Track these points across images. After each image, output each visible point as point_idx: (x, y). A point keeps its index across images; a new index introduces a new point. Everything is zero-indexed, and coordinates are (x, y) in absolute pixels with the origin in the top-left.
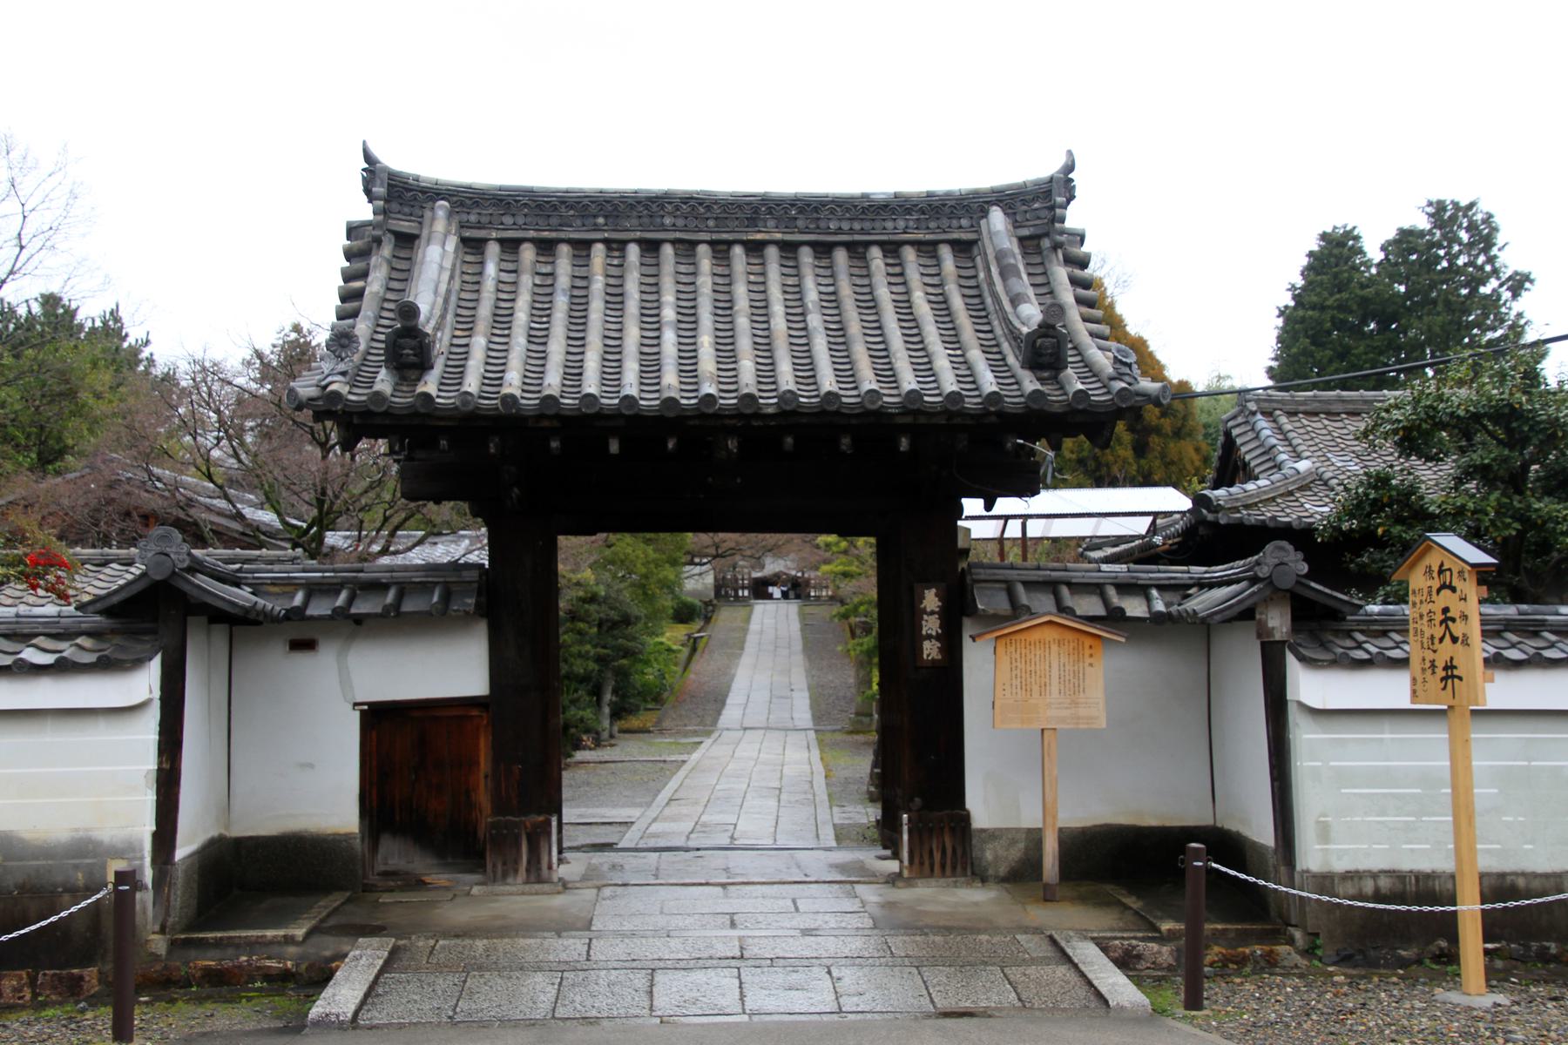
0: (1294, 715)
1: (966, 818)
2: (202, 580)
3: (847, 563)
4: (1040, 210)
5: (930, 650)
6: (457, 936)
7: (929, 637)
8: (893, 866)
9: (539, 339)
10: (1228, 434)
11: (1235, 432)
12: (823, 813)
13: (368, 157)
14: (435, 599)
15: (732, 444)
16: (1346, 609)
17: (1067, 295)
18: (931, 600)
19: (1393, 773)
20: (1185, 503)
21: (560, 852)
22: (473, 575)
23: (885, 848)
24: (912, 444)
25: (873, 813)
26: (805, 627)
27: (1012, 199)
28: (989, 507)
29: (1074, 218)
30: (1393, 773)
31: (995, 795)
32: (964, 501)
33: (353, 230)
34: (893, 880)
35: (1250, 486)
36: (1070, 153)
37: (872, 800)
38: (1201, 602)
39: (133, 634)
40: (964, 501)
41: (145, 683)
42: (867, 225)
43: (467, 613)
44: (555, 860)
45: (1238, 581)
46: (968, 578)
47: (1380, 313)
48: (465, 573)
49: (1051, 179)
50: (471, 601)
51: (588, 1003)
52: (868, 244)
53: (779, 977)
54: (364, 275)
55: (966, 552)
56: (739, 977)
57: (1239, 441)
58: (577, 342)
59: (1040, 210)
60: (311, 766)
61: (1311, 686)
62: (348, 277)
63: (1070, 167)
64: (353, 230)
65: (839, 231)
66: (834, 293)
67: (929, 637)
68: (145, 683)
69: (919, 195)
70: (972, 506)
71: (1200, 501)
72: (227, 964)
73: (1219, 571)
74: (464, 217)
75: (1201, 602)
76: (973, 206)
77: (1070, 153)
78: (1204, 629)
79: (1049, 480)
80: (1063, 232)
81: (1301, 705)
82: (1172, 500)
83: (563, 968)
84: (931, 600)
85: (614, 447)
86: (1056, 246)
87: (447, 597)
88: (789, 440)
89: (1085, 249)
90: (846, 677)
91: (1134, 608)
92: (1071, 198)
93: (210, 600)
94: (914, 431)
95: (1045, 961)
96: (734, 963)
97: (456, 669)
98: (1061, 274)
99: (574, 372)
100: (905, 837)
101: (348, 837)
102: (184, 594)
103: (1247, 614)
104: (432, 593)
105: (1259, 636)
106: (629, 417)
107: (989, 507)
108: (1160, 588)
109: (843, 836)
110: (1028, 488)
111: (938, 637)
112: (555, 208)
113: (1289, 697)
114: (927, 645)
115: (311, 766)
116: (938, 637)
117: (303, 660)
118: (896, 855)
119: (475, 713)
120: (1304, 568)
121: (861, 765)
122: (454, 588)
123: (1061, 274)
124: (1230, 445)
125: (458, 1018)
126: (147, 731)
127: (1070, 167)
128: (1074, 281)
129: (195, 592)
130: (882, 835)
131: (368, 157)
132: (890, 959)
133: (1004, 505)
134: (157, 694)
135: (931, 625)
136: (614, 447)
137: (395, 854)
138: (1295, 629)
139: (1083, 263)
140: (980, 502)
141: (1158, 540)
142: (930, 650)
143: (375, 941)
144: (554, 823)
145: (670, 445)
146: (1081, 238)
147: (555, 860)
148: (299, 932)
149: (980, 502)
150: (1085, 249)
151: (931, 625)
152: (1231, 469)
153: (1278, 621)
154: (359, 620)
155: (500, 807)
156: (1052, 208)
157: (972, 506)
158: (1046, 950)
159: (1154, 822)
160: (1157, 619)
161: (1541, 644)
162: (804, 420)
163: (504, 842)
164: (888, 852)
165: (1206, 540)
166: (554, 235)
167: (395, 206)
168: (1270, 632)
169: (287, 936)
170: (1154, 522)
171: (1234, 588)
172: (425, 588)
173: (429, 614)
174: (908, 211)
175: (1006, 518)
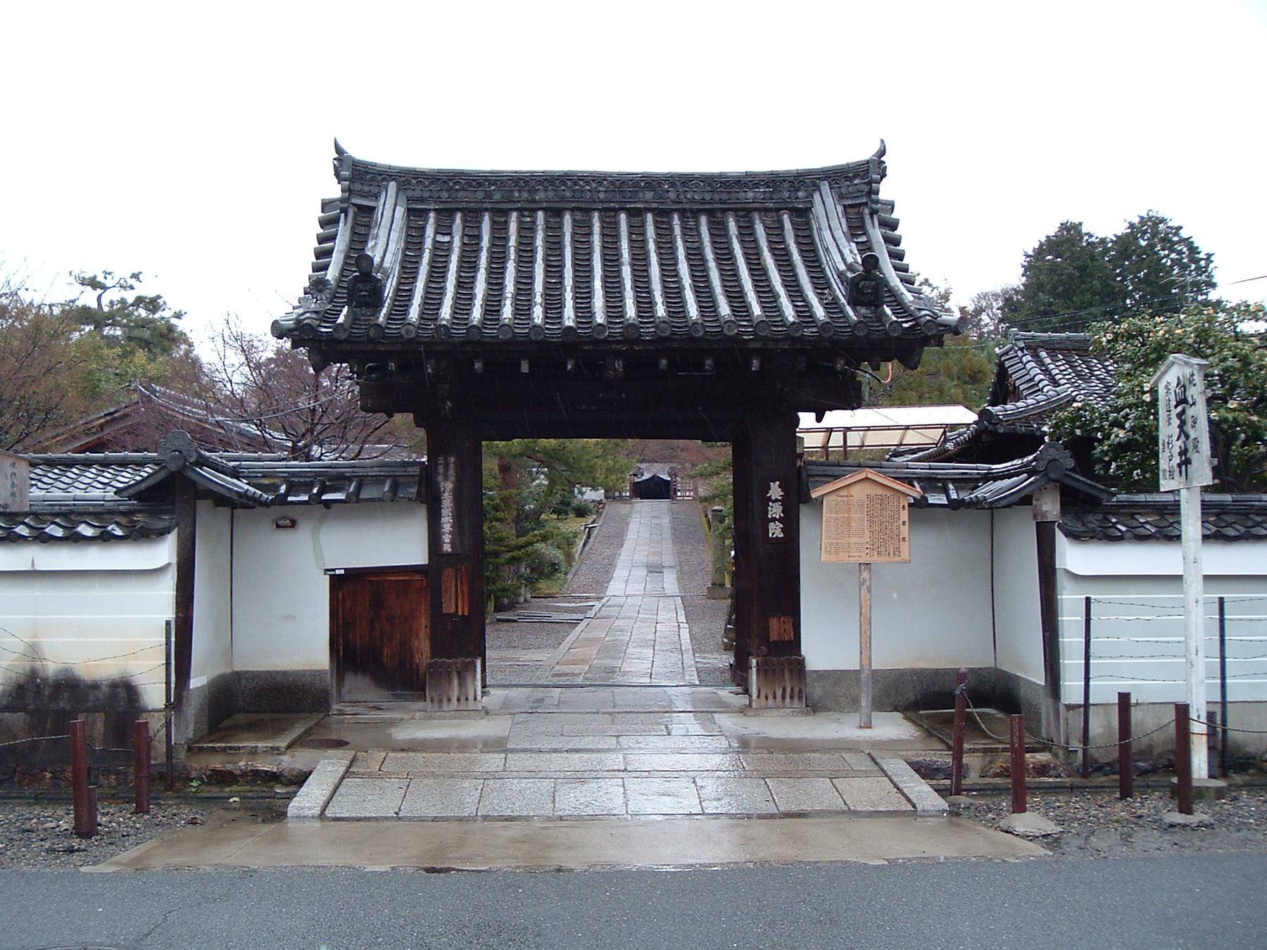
0: (1062, 582)
1: (801, 663)
2: (206, 472)
3: (703, 469)
4: (859, 186)
5: (775, 530)
6: (403, 750)
7: (774, 520)
8: (744, 700)
9: (465, 285)
10: (1001, 365)
11: (1007, 364)
12: (689, 659)
13: (338, 149)
14: (386, 489)
15: (619, 365)
16: (1102, 496)
17: (882, 252)
18: (775, 491)
19: (1157, 623)
20: (969, 417)
21: (484, 687)
22: (416, 471)
23: (738, 685)
24: (761, 365)
25: (728, 659)
26: (674, 520)
27: (837, 176)
28: (819, 419)
29: (886, 191)
30: (1157, 623)
31: (825, 643)
32: (800, 414)
33: (326, 205)
34: (742, 711)
35: (1020, 404)
36: (882, 141)
37: (727, 648)
38: (986, 491)
39: (155, 514)
40: (800, 414)
41: (164, 552)
42: (725, 196)
43: (410, 499)
44: (479, 693)
45: (1017, 475)
46: (804, 475)
47: (1108, 285)
48: (409, 469)
49: (868, 162)
50: (414, 490)
51: (504, 805)
52: (724, 211)
53: (656, 784)
54: (332, 238)
55: (801, 455)
56: (623, 786)
57: (1010, 371)
58: (495, 283)
59: (859, 186)
60: (293, 618)
61: (1075, 557)
62: (321, 240)
63: (882, 152)
64: (326, 205)
65: (703, 201)
66: (698, 248)
67: (774, 520)
68: (164, 552)
69: (765, 174)
70: (807, 419)
71: (983, 414)
72: (229, 767)
73: (998, 467)
74: (410, 193)
75: (986, 491)
76: (805, 181)
77: (882, 141)
78: (991, 508)
79: (866, 397)
80: (877, 202)
81: (1067, 571)
82: (963, 415)
83: (488, 776)
84: (775, 491)
85: (525, 368)
86: (873, 213)
87: (395, 487)
88: (664, 362)
89: (894, 216)
90: (707, 556)
91: (936, 499)
92: (883, 176)
93: (212, 487)
94: (763, 354)
95: (866, 774)
96: (621, 774)
97: (399, 544)
98: (876, 234)
99: (492, 308)
100: (754, 677)
101: (321, 672)
102: (194, 483)
103: (1026, 500)
104: (384, 484)
105: (1035, 517)
106: (537, 342)
107: (819, 419)
108: (954, 481)
109: (705, 675)
110: (852, 402)
111: (780, 520)
112: (480, 184)
113: (1059, 565)
114: (771, 526)
115: (293, 618)
116: (780, 520)
117: (285, 537)
118: (747, 691)
119: (418, 577)
120: (1070, 463)
121: (718, 625)
122: (401, 480)
123: (876, 234)
124: (1003, 373)
125: (401, 814)
126: (166, 590)
127: (882, 152)
128: (888, 240)
129: (202, 481)
130: (733, 676)
131: (338, 149)
132: (744, 775)
133: (835, 418)
134: (174, 561)
135: (776, 510)
136: (525, 368)
137: (358, 686)
138: (1063, 512)
139: (893, 225)
140: (813, 415)
141: (950, 446)
142: (775, 530)
143: (339, 752)
144: (479, 663)
145: (569, 367)
146: (891, 206)
147: (479, 693)
148: (283, 744)
149: (813, 415)
150: (894, 216)
151: (776, 510)
152: (1004, 390)
153: (1050, 507)
154: (327, 504)
155: (435, 652)
156: (870, 183)
157: (807, 419)
158: (869, 765)
159: (907, 667)
160: (954, 505)
161: (1250, 523)
162: (676, 345)
163: (440, 674)
164: (740, 690)
165: (987, 444)
166: (479, 205)
167: (357, 186)
168: (1044, 514)
169: (267, 753)
170: (944, 433)
171: (1007, 482)
172: (379, 480)
173: (381, 500)
174: (757, 185)
175: (830, 431)
